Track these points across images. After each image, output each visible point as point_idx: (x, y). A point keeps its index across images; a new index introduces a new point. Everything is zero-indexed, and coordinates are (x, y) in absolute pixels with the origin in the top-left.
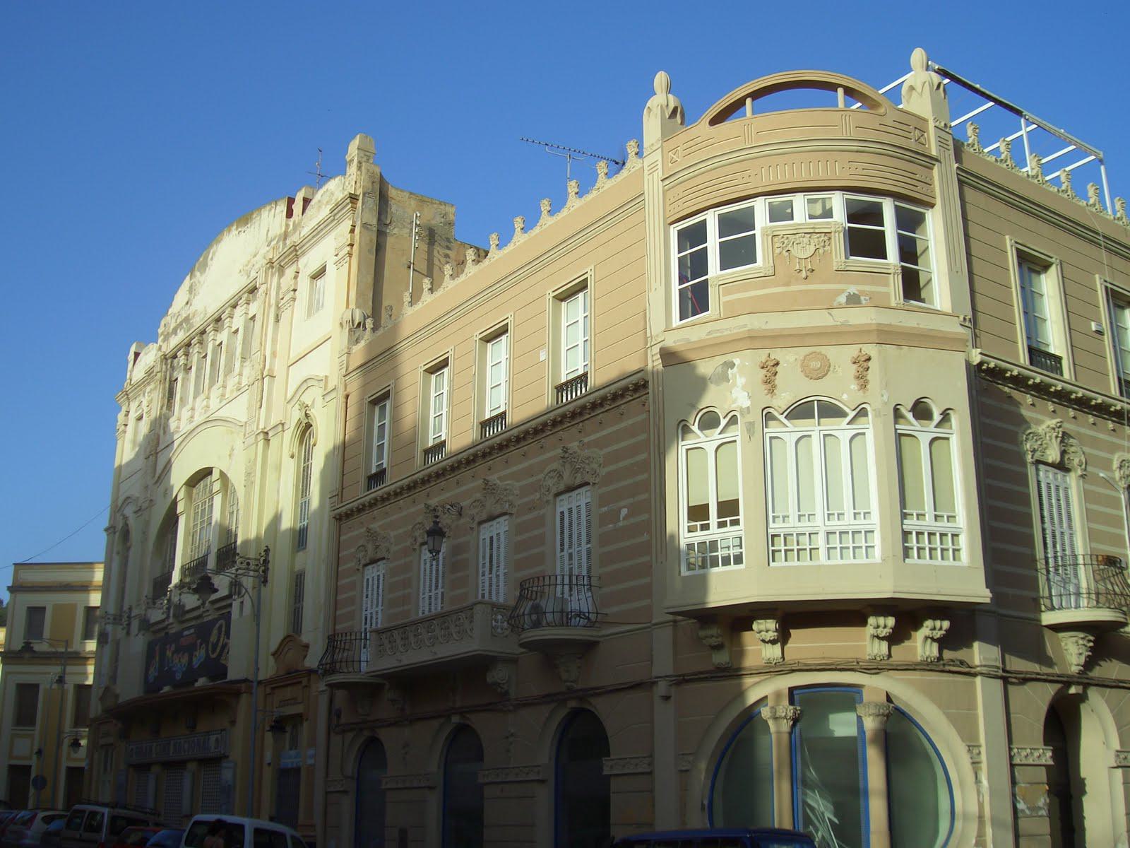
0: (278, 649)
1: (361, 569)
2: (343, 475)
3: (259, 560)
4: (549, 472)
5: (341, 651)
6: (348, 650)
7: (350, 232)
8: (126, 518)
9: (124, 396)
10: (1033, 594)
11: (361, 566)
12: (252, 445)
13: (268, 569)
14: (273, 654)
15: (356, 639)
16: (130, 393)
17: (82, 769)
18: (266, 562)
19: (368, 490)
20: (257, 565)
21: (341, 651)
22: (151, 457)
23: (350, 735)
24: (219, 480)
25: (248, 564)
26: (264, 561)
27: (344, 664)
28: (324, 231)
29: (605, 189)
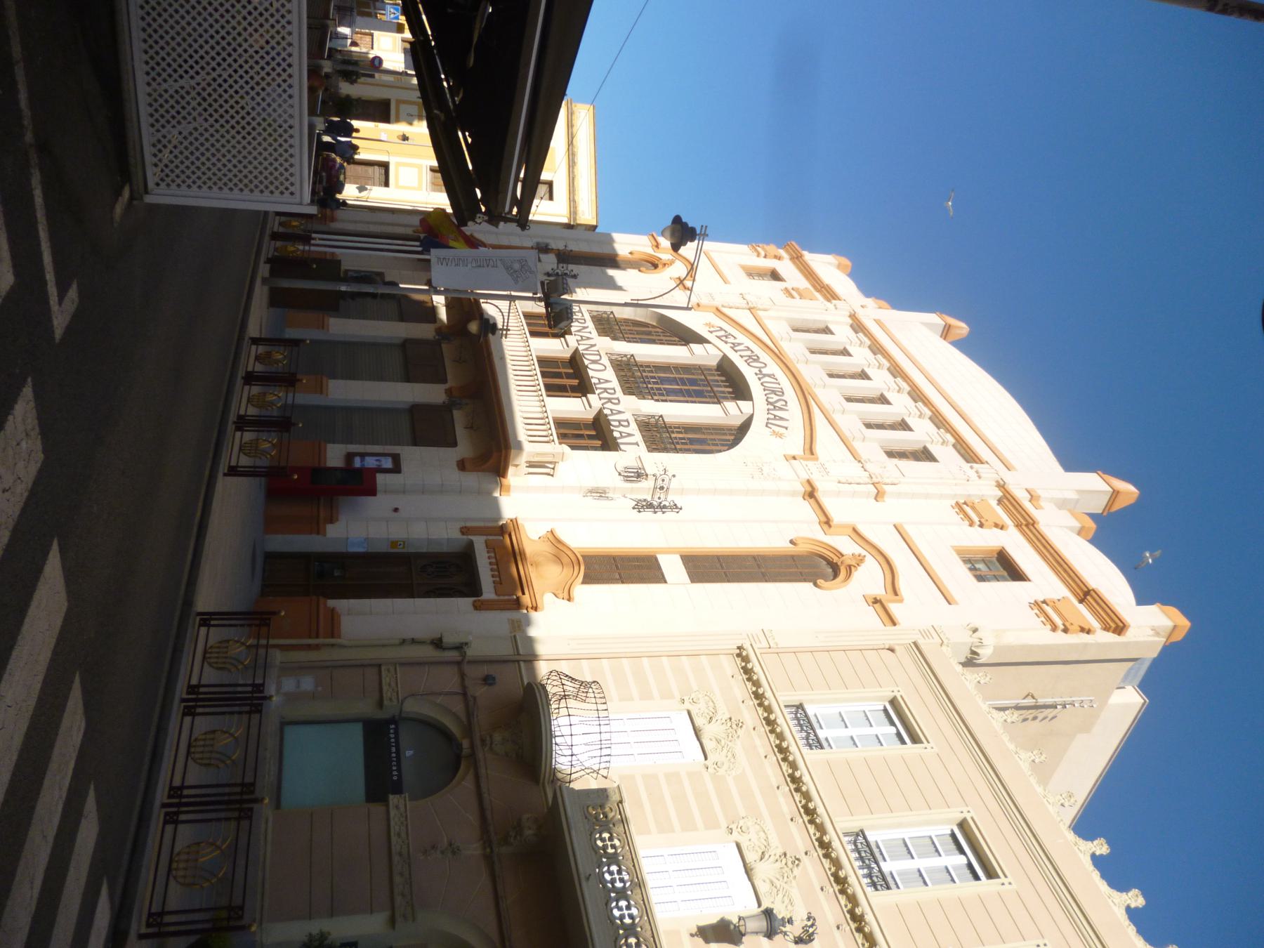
18: (662, 508)
23: (458, 707)
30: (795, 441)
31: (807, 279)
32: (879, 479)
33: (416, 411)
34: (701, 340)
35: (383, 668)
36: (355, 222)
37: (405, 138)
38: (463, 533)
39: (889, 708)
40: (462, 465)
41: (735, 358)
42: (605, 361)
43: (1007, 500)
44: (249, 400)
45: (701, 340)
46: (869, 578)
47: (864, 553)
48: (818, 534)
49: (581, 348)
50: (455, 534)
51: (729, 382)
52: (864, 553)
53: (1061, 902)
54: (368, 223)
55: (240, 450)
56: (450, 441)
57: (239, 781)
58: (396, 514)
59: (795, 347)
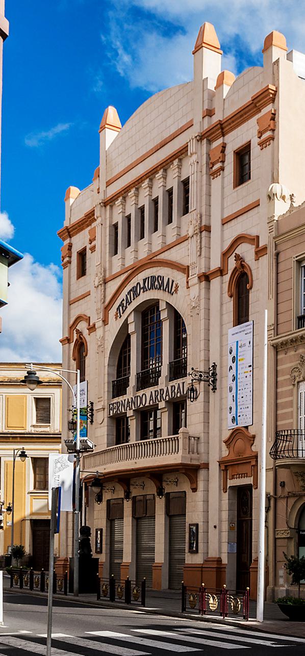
0: (229, 439)
1: (296, 384)
2: (277, 314)
3: (209, 373)
4: (295, 368)
5: (285, 441)
6: (290, 441)
7: (221, 152)
8: (80, 333)
9: (225, 127)
10: (230, 501)
11: (296, 382)
12: (100, 327)
13: (216, 380)
14: (225, 442)
15: (294, 435)
16: (72, 231)
17: (48, 521)
18: (214, 374)
19: (299, 328)
20: (207, 377)
21: (285, 441)
22: (100, 286)
23: (292, 501)
24: (134, 323)
25: (201, 376)
26: (212, 373)
27: (282, 452)
28: (252, 111)
29: (293, 212)
30: (179, 278)
31: (82, 229)
32: (198, 227)
33: (169, 515)
34: (125, 325)
35: (277, 537)
36: (67, 546)
37: (136, 463)
38: (226, 492)
39: (59, 436)
40: (195, 490)
41: (135, 304)
42: (140, 393)
43: (207, 136)
44: (136, 601)
45: (125, 325)
46: (246, 251)
47: (234, 254)
48: (227, 278)
49: (134, 409)
50: (226, 496)
51: (148, 314)
52: (234, 254)
53: (5, 474)
54: (67, 538)
55: (193, 608)
56: (183, 496)
57: (10, 580)
58: (217, 527)
59: (129, 257)
